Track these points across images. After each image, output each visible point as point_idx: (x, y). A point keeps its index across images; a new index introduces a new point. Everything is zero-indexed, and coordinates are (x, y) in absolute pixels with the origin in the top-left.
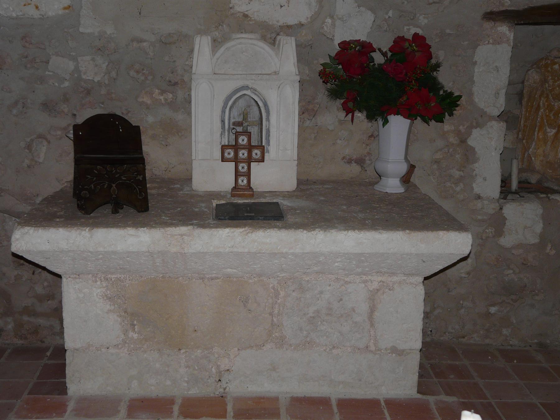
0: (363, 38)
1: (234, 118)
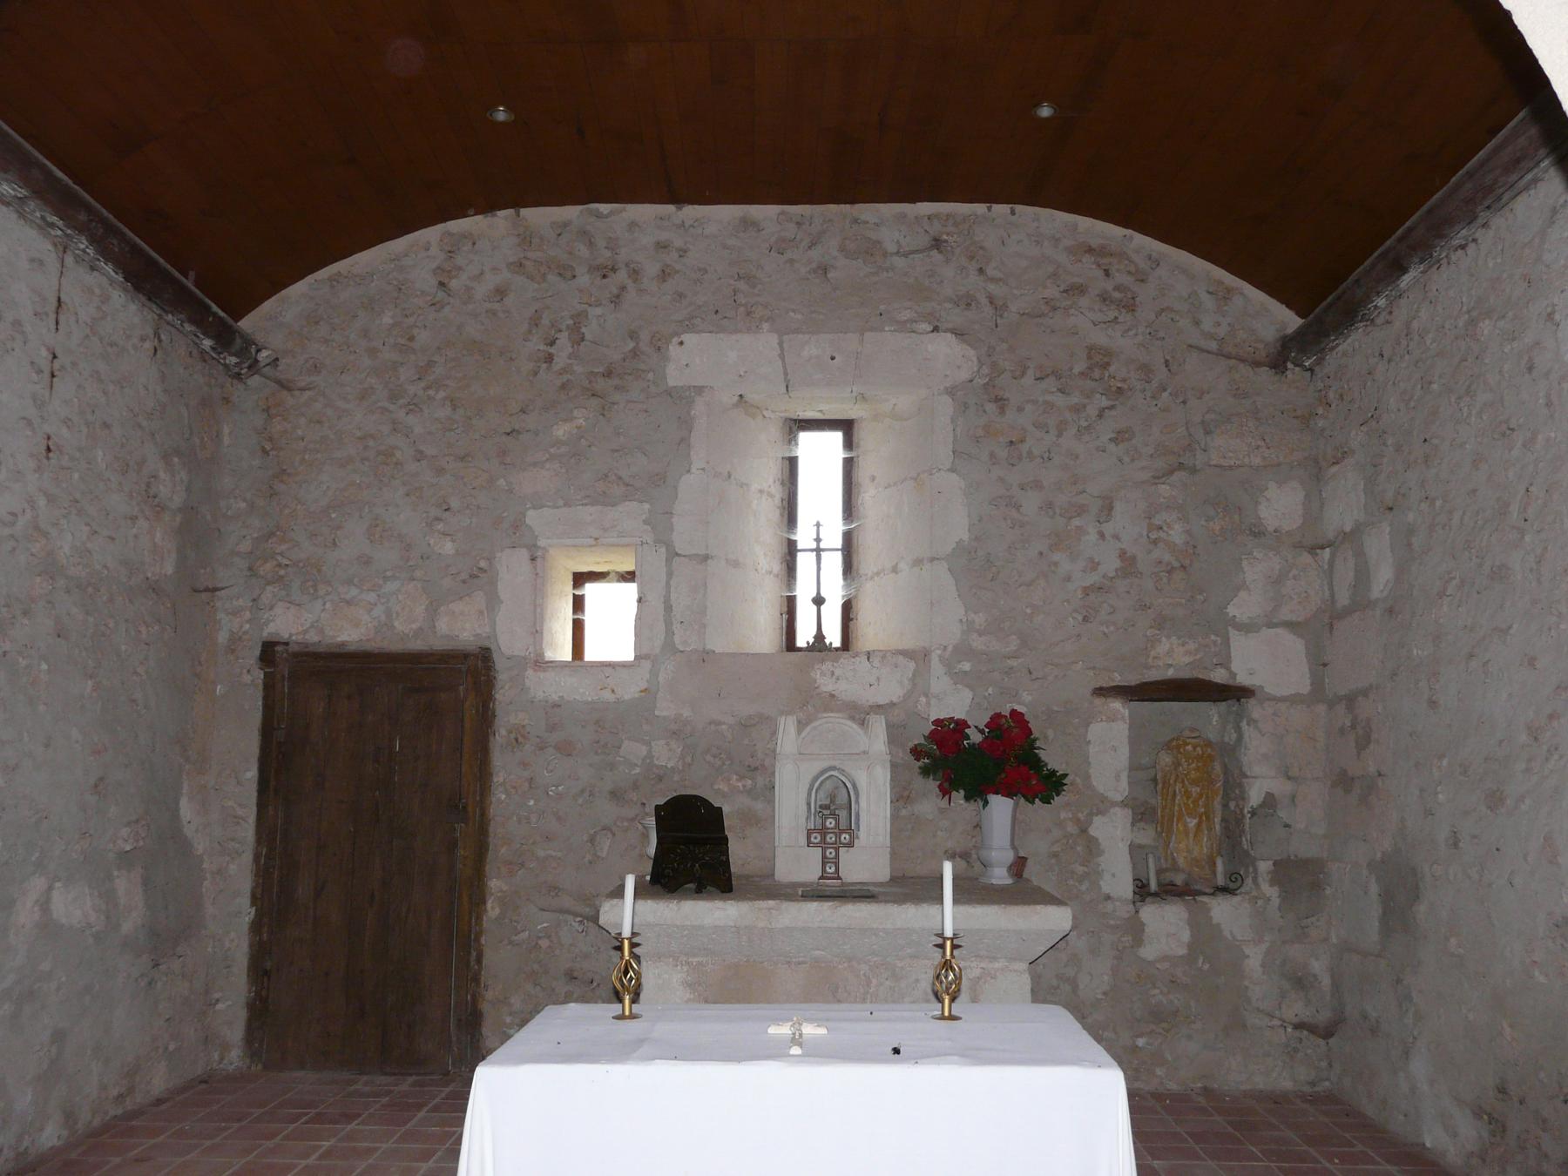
0: (958, 715)
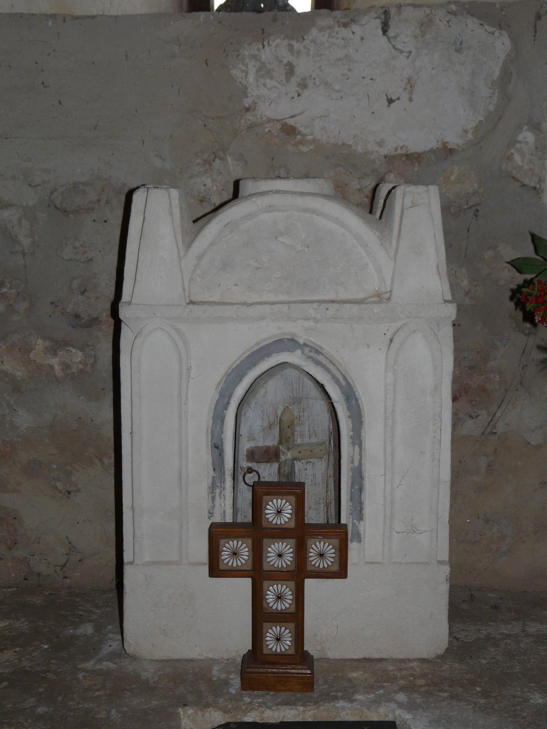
1: (251, 438)
